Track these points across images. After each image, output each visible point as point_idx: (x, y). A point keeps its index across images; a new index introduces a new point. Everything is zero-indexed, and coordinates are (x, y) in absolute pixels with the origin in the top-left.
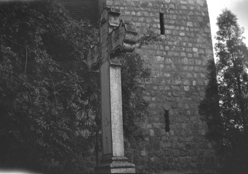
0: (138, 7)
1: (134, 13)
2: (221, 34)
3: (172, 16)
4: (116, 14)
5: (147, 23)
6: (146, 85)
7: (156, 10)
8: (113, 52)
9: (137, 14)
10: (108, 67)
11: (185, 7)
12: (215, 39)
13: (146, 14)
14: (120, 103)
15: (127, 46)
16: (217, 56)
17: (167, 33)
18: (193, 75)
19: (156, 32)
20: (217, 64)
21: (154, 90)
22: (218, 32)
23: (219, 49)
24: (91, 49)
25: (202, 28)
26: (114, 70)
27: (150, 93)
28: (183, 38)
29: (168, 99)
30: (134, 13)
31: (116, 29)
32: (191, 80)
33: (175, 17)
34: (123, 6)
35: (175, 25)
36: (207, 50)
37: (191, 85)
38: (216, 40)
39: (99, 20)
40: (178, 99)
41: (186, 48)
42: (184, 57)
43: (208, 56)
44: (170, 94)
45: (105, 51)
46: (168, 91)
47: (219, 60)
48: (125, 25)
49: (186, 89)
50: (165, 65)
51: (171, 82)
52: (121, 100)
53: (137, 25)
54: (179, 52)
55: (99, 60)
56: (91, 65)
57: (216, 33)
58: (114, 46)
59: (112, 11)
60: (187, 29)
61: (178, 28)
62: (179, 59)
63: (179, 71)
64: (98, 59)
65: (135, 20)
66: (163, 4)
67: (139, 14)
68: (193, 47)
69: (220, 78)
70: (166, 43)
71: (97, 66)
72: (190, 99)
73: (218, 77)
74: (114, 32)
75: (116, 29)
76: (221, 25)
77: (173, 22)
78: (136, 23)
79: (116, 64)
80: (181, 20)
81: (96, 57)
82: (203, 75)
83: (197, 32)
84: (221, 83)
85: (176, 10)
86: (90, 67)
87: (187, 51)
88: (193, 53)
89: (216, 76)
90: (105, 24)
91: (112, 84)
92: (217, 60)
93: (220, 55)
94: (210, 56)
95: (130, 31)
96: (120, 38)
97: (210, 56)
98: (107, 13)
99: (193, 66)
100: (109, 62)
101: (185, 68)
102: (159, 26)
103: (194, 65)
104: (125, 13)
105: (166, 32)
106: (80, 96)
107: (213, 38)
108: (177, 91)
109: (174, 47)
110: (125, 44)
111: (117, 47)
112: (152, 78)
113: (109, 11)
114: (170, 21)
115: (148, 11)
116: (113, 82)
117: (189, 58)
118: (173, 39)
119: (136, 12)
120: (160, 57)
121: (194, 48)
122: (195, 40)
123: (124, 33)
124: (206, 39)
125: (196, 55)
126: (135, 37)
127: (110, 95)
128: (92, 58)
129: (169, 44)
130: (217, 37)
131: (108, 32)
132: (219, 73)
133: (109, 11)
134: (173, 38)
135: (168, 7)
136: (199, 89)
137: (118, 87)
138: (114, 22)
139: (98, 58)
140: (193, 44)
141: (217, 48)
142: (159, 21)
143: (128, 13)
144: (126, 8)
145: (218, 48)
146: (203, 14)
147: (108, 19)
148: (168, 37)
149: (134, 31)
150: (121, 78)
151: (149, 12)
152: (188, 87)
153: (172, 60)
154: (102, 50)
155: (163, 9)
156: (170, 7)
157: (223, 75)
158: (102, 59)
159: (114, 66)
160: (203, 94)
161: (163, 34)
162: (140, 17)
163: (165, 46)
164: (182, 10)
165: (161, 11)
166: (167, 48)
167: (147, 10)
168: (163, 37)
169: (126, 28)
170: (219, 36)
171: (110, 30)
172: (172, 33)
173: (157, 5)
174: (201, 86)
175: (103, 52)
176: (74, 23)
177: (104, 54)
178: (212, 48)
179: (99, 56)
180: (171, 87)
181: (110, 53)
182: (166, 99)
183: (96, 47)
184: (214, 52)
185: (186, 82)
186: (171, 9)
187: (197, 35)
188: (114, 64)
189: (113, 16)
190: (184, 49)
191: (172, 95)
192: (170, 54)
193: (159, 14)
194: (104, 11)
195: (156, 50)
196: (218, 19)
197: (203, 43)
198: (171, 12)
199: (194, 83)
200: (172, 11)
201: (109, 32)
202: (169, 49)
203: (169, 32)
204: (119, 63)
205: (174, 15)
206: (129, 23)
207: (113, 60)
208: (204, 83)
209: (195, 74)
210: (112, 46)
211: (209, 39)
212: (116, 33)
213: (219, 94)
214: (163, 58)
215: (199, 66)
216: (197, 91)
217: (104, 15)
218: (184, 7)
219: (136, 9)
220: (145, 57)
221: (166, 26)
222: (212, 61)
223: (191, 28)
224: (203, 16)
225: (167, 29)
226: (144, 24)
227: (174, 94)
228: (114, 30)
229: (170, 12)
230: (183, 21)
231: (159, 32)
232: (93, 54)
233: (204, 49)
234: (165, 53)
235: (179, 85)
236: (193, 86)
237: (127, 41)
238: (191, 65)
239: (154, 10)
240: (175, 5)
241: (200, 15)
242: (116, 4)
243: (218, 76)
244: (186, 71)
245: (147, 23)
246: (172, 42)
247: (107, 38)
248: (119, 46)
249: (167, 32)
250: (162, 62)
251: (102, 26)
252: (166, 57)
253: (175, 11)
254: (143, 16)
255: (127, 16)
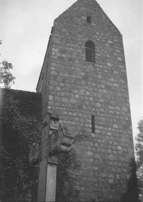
0: (74, 109)
1: (70, 114)
2: (141, 137)
3: (101, 118)
4: (56, 119)
5: (81, 123)
6: (77, 175)
7: (89, 112)
8: (51, 151)
9: (73, 114)
10: (46, 165)
11: (113, 112)
12: (136, 140)
13: (80, 115)
14: (54, 197)
15: (64, 148)
16: (137, 155)
17: (97, 133)
18: (117, 169)
19: (88, 130)
20: (137, 162)
21: (83, 181)
22: (139, 134)
23: (139, 149)
24: (33, 146)
25: (125, 130)
26: (51, 168)
27: (80, 183)
28: (110, 137)
29: (95, 189)
30: (70, 114)
31: (55, 132)
32: (115, 174)
33: (104, 119)
34: (62, 107)
35: (104, 126)
36: (129, 148)
37: (115, 178)
38: (137, 141)
39: (42, 123)
40: (103, 190)
41: (112, 146)
42: (110, 154)
43: (130, 154)
44: (96, 185)
45: (45, 149)
46: (95, 182)
47: (139, 158)
48: (63, 129)
49: (111, 181)
50: (94, 159)
51: (98, 174)
52: (55, 194)
53: (72, 124)
54: (106, 149)
55: (39, 157)
56: (32, 160)
57: (137, 135)
58: (53, 146)
59: (53, 116)
60: (114, 130)
61: (106, 128)
62: (106, 155)
63: (105, 165)
64: (38, 156)
65: (71, 119)
66: (95, 108)
67: (75, 114)
68: (117, 146)
69: (139, 174)
70: (96, 141)
71: (38, 161)
72: (114, 191)
73: (138, 173)
74: (54, 134)
75: (56, 132)
76: (142, 129)
77: (103, 123)
78: (72, 122)
79: (53, 162)
80: (109, 122)
81: (37, 154)
82: (125, 170)
83: (121, 133)
84: (141, 178)
85: (105, 113)
86: (31, 162)
87: (113, 148)
88: (117, 150)
89: (136, 172)
90: (47, 126)
91: (48, 179)
92: (138, 158)
93: (140, 154)
94: (131, 154)
95: (67, 135)
96: (58, 140)
97: (131, 154)
98: (49, 118)
99: (117, 161)
100: (47, 160)
101: (111, 163)
102: (91, 126)
103: (118, 161)
104: (63, 112)
105: (96, 131)
106: (23, 181)
107: (134, 139)
108: (103, 183)
109: (102, 144)
110: (62, 146)
111: (55, 148)
112: (82, 170)
113: (50, 116)
114: (100, 122)
115: (82, 113)
116: (49, 178)
117: (114, 155)
118: (102, 138)
119: (72, 112)
120: (90, 152)
121: (118, 146)
122: (119, 140)
123: (62, 137)
124: (128, 140)
125: (120, 153)
126: (71, 141)
127: (46, 189)
128: (34, 154)
129: (98, 142)
130: (138, 138)
131: (49, 134)
132: (139, 169)
133: (50, 116)
134: (102, 137)
135: (99, 110)
136: (122, 182)
137: (53, 183)
138: (54, 125)
139: (38, 155)
140: (118, 143)
141: (138, 148)
142: (91, 122)
143: (65, 113)
144: (64, 109)
145: (139, 148)
146: (127, 119)
147: (49, 122)
148: (97, 135)
149: (70, 136)
150: (56, 175)
151: (83, 113)
152: (112, 180)
153: (100, 156)
154: (42, 148)
155: (95, 112)
156: (100, 111)
157: (142, 171)
158: (41, 157)
159: (52, 164)
160: (125, 187)
161: (94, 133)
162: (75, 117)
163: (95, 143)
164: (110, 114)
165: (93, 114)
166: (96, 145)
167: (82, 111)
168: (93, 135)
169: (64, 132)
170: (139, 138)
171: (51, 132)
172: (101, 132)
173: (90, 108)
174: (123, 180)
175: (43, 150)
176: (23, 119)
177: (44, 152)
178: (133, 147)
179: (39, 154)
180: (98, 179)
181: (49, 152)
182: (93, 190)
183: (37, 145)
184: (135, 151)
185: (111, 176)
186: (101, 112)
187: (122, 135)
188: (52, 162)
189: (53, 120)
190: (110, 147)
191: (99, 186)
192: (99, 150)
193: (91, 116)
194: (46, 116)
195: (87, 146)
196: (139, 124)
197: (126, 143)
198: (101, 115)
199: (118, 176)
200: (102, 114)
201: (50, 133)
202: (98, 146)
203: (98, 131)
204: (56, 162)
205: (103, 118)
206: (66, 128)
207: (51, 159)
208: (126, 177)
209: (119, 169)
210: (51, 146)
211: (131, 139)
212: (55, 135)
213: (139, 188)
214: (93, 154)
215: (122, 162)
216: (120, 184)
217: (46, 119)
218: (112, 112)
219: (72, 110)
220: (78, 152)
221: (96, 126)
222: (133, 159)
223: (116, 130)
224: (127, 120)
225: (97, 129)
226: (78, 123)
227: (101, 186)
228: (54, 133)
229: (100, 115)
230: (111, 123)
231: (91, 130)
232: (34, 151)
233: (127, 148)
234: (94, 149)
235: (105, 178)
236: (116, 179)
237: (64, 144)
238: (115, 161)
239: (87, 112)
240: (104, 109)
241: (124, 119)
242: (56, 105)
243: (138, 172)
244: (111, 166)
245: (81, 123)
246: (100, 140)
247: (47, 139)
248: (57, 147)
249: (97, 131)
250: (91, 157)
251: (44, 127)
252: (95, 153)
253: (104, 115)
254: (78, 116)
255: (65, 115)
